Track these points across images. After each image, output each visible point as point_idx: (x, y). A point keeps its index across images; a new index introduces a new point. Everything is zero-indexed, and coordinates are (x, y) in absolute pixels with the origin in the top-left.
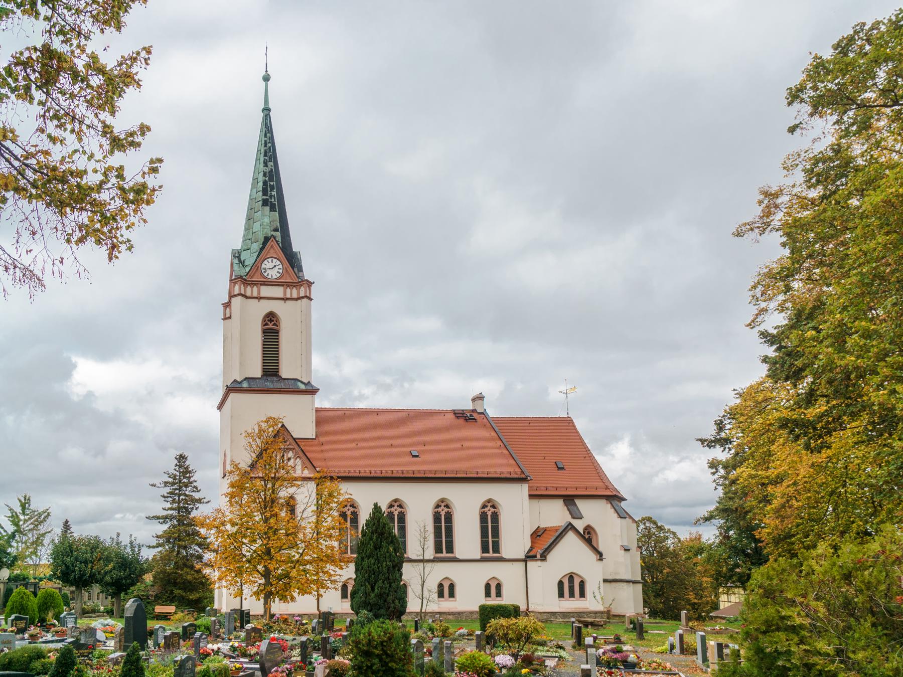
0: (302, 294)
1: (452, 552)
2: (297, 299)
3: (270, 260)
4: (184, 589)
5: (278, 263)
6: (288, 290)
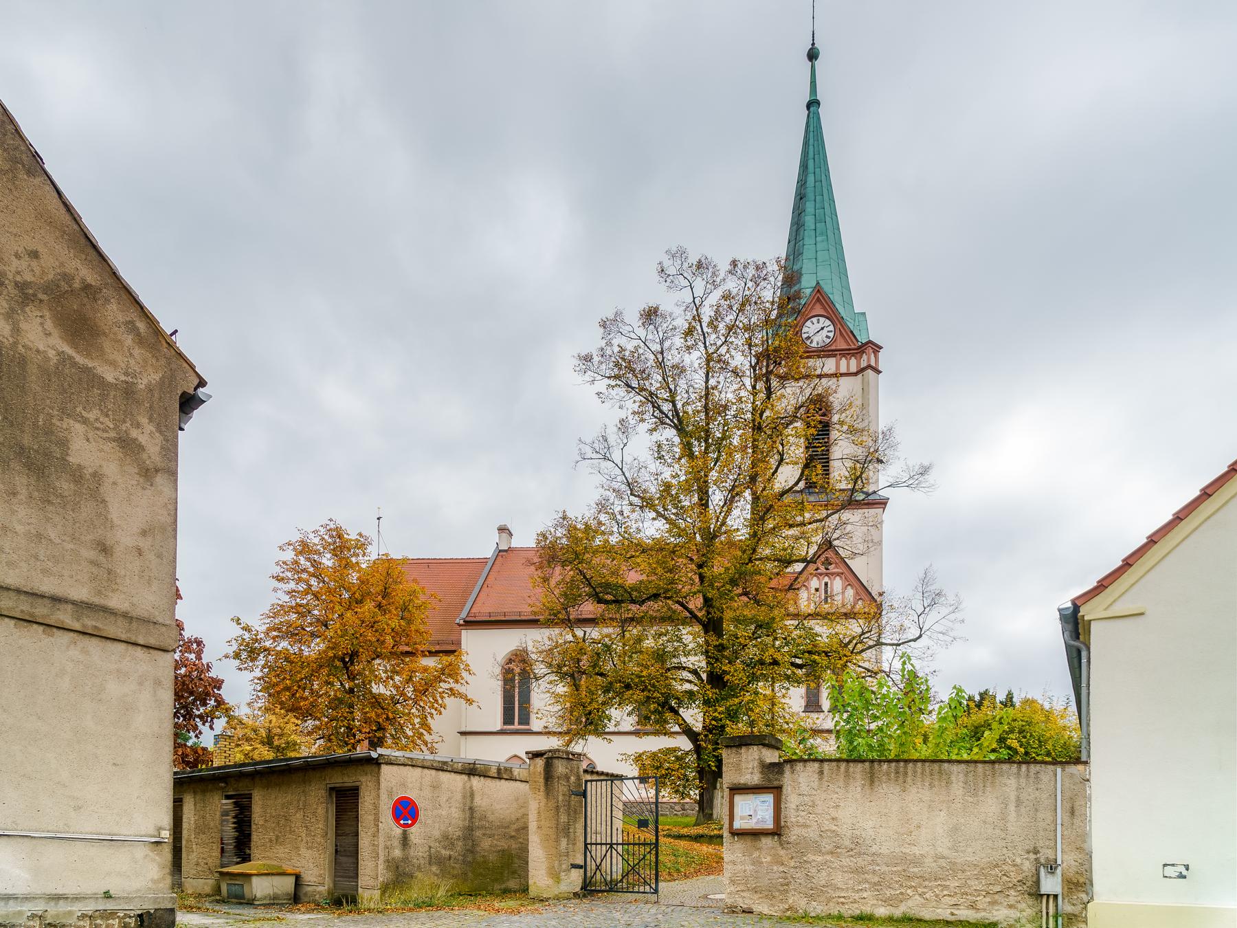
0: (864, 364)
1: (528, 724)
2: (856, 374)
3: (814, 320)
5: (828, 322)
6: (843, 362)
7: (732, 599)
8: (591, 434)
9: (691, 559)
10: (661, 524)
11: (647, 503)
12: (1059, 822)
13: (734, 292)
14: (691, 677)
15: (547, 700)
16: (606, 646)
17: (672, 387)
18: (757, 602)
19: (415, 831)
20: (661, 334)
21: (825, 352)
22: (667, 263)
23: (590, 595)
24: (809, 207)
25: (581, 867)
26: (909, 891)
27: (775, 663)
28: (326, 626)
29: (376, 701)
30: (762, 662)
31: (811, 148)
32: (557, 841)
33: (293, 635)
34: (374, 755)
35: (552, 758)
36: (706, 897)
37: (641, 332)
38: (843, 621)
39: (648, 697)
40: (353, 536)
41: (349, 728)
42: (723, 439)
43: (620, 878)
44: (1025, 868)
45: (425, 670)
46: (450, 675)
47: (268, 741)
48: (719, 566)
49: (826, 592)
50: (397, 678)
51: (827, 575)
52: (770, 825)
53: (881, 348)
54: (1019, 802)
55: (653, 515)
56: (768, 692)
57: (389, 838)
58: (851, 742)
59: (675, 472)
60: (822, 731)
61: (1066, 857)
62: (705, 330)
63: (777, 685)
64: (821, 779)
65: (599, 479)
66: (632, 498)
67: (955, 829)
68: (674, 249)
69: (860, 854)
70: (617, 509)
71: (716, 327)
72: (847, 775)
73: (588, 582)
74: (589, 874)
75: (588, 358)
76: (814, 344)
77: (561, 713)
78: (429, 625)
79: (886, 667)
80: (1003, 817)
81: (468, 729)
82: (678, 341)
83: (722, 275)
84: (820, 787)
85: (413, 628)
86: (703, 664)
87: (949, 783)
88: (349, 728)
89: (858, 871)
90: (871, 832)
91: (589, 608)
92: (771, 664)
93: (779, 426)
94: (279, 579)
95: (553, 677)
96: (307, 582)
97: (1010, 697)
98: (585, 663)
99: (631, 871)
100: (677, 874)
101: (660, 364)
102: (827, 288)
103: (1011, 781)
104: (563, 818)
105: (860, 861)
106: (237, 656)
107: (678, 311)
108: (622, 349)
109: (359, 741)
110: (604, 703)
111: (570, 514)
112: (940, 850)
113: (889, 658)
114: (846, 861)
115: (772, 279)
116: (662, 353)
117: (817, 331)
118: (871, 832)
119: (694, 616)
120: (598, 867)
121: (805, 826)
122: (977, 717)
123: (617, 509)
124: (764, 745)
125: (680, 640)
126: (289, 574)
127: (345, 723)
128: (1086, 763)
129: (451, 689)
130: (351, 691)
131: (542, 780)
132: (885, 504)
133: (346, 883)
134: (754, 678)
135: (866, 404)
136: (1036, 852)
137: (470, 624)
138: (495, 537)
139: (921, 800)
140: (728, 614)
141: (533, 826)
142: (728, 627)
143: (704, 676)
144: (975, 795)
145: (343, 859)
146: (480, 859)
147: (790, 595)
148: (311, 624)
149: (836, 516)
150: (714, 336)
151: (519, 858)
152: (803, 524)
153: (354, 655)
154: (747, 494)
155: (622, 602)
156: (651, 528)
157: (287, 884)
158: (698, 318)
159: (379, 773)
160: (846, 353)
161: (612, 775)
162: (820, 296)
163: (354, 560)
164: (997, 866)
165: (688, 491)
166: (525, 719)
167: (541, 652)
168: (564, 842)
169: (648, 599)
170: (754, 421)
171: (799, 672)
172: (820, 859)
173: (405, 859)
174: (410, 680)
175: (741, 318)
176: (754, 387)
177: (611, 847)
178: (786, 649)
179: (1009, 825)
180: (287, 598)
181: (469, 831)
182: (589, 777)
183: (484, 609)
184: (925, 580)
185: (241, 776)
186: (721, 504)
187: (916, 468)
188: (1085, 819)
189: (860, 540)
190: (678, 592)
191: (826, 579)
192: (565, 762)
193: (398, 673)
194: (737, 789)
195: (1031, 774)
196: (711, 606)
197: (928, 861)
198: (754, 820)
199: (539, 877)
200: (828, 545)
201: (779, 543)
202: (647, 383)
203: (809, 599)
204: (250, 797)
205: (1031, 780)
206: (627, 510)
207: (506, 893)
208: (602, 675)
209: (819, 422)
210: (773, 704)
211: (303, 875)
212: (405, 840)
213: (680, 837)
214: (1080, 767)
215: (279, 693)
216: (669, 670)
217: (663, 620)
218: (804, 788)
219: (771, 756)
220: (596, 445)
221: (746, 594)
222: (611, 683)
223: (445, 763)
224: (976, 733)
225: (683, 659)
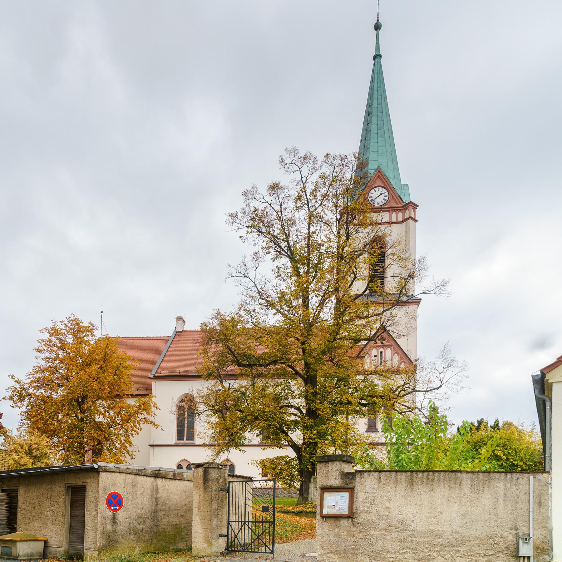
0: (407, 216)
1: (193, 440)
2: (402, 222)
3: (376, 189)
4: (188, 415)
5: (385, 191)
6: (394, 215)
7: (323, 364)
8: (236, 261)
9: (298, 339)
10: (279, 317)
11: (270, 304)
12: (531, 510)
13: (327, 174)
14: (295, 412)
15: (205, 426)
16: (242, 393)
17: (287, 232)
18: (339, 366)
19: (121, 514)
20: (281, 200)
21: (382, 209)
22: (285, 156)
23: (233, 362)
24: (374, 119)
25: (224, 536)
26: (434, 554)
27: (349, 403)
28: (67, 380)
29: (98, 426)
30: (341, 403)
31: (376, 84)
32: (211, 520)
33: (47, 385)
34: (96, 466)
35: (208, 468)
36: (304, 555)
37: (269, 199)
38: (391, 376)
39: (269, 425)
40: (86, 324)
41: (81, 443)
42: (318, 264)
43: (250, 542)
44: (509, 539)
45: (129, 406)
46: (144, 410)
47: (29, 453)
48: (315, 344)
49: (381, 359)
50: (111, 412)
51: (382, 347)
52: (346, 511)
53: (418, 206)
54: (505, 497)
55: (274, 311)
56: (344, 421)
57: (104, 518)
58: (398, 457)
59: (287, 285)
60: (377, 444)
61: (535, 532)
62: (309, 197)
63: (350, 417)
64: (379, 483)
65: (241, 289)
66: (261, 300)
67: (465, 514)
68: (290, 148)
69: (403, 530)
70: (251, 308)
71: (315, 196)
72: (396, 481)
73: (233, 353)
74: (230, 540)
75: (234, 215)
76: (376, 204)
77: (213, 435)
78: (131, 378)
79: (419, 405)
80: (496, 507)
81: (155, 443)
82: (291, 204)
83: (320, 163)
84: (378, 488)
85: (122, 381)
86: (304, 404)
87: (461, 485)
88: (81, 443)
89: (401, 541)
90: (411, 516)
91: (233, 369)
92: (346, 404)
93: (354, 256)
94: (39, 351)
95: (209, 412)
96: (56, 352)
97: (497, 423)
98: (229, 403)
99: (257, 537)
100: (286, 539)
101: (280, 218)
102: (384, 169)
103: (501, 484)
104: (215, 506)
105: (404, 535)
106: (11, 398)
107: (292, 186)
108: (256, 210)
109: (86, 451)
110: (241, 429)
111: (222, 312)
112: (455, 527)
113: (420, 400)
114: (394, 535)
115: (351, 166)
116: (281, 211)
117: (378, 196)
118: (411, 516)
119: (297, 373)
120: (236, 536)
121: (369, 512)
122: (476, 436)
123: (251, 308)
124: (343, 461)
125: (289, 388)
126: (45, 348)
127: (78, 440)
128: (549, 473)
129: (145, 419)
130: (82, 420)
131: (201, 482)
132: (419, 302)
133: (76, 546)
134: (336, 413)
135: (408, 240)
136: (516, 529)
137: (158, 378)
138: (174, 323)
139: (443, 496)
140: (320, 373)
141: (195, 510)
142: (320, 380)
143: (304, 411)
144: (478, 493)
145: (75, 531)
146: (161, 530)
147: (359, 360)
148: (58, 378)
149: (389, 312)
150: (314, 201)
151: (186, 529)
152: (368, 317)
153: (84, 398)
154: (333, 299)
155: (254, 365)
156: (273, 319)
157: (40, 546)
158: (304, 190)
159: (98, 477)
160: (396, 209)
161: (246, 477)
162: (380, 174)
163: (86, 339)
164: (491, 538)
165: (297, 297)
166: (191, 437)
167: (202, 396)
168: (215, 521)
169: (270, 364)
170: (338, 253)
171: (364, 408)
172: (378, 533)
173: (114, 531)
174: (119, 413)
175: (331, 189)
176: (339, 233)
177: (245, 524)
178: (356, 394)
179: (499, 512)
180: (43, 363)
181: (155, 512)
182: (231, 479)
183: (166, 369)
184: (445, 351)
185: (12, 477)
186: (317, 304)
187: (440, 282)
188: (548, 509)
189: (404, 327)
190: (289, 359)
191: (382, 349)
192: (216, 470)
193: (111, 409)
194: (326, 489)
195: (514, 480)
196: (309, 368)
197: (447, 535)
198: (336, 508)
199: (198, 542)
200: (383, 328)
201: (352, 328)
202: (271, 230)
203: (370, 363)
204: (17, 491)
205: (514, 483)
206: (257, 308)
207: (177, 551)
208: (240, 411)
209: (378, 250)
210: (347, 429)
211: (49, 541)
212: (114, 520)
213: (287, 512)
214: (545, 475)
215: (36, 421)
216: (282, 407)
217: (279, 375)
218: (368, 488)
219: (348, 468)
220: (239, 268)
221: (331, 360)
222: (245, 416)
223: (140, 470)
224: (477, 446)
225: (291, 401)
